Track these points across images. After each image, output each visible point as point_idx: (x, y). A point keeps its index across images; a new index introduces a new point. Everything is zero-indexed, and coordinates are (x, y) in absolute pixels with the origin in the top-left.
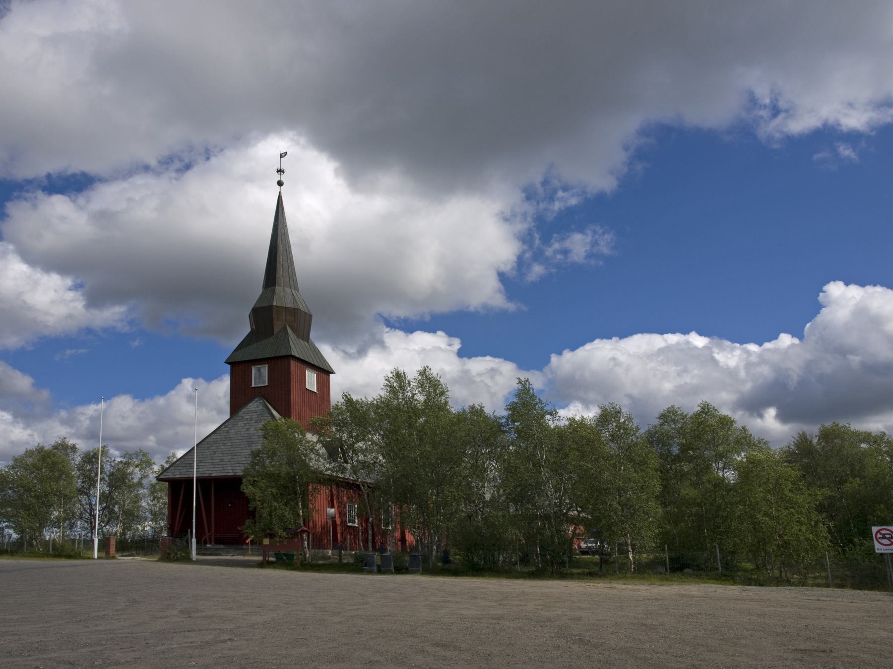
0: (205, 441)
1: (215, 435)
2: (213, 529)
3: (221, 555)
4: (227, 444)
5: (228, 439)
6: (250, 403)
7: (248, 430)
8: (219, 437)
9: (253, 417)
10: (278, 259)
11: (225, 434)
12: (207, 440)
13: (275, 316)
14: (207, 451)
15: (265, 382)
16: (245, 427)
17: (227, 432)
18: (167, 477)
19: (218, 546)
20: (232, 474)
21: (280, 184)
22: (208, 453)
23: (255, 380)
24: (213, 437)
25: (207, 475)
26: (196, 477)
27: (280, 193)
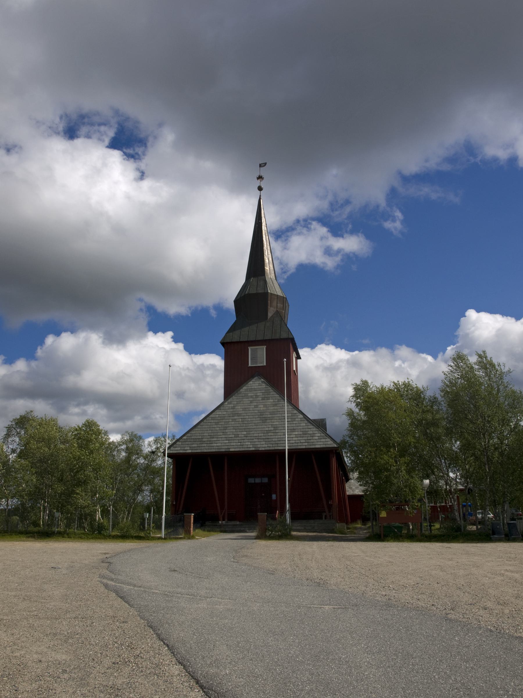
0: (210, 416)
1: (218, 411)
2: (226, 507)
3: (164, 531)
4: (237, 420)
5: (236, 415)
6: (250, 381)
7: (256, 406)
8: (225, 413)
9: (258, 394)
10: (265, 253)
11: (232, 410)
12: (211, 416)
13: (269, 304)
14: (216, 426)
15: (263, 362)
16: (252, 404)
17: (233, 408)
18: (176, 452)
19: (233, 523)
20: (254, 449)
21: (260, 189)
22: (218, 429)
23: (251, 359)
24: (218, 412)
25: (224, 450)
26: (288, 449)
27: (260, 196)
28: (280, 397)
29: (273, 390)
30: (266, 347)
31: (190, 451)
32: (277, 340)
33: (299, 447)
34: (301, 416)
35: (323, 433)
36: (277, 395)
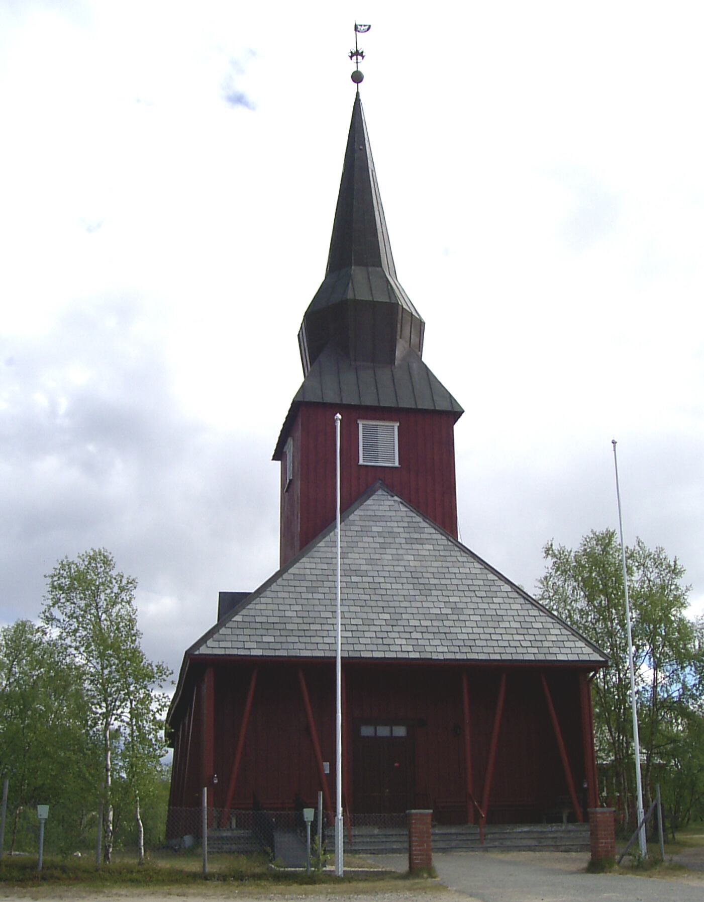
28: (448, 539)
29: (429, 524)
30: (398, 424)
31: (259, 653)
32: (424, 412)
33: (520, 657)
34: (507, 588)
35: (566, 629)
36: (439, 536)
